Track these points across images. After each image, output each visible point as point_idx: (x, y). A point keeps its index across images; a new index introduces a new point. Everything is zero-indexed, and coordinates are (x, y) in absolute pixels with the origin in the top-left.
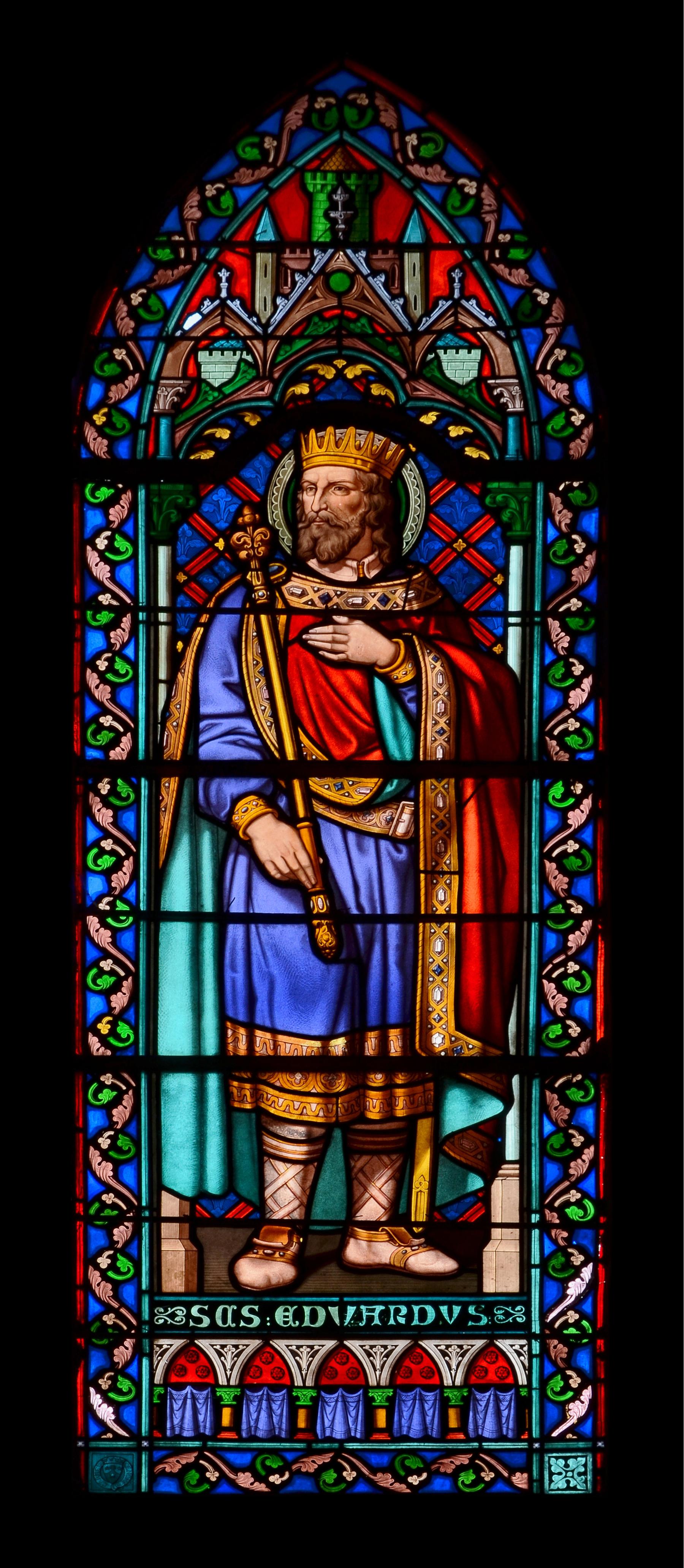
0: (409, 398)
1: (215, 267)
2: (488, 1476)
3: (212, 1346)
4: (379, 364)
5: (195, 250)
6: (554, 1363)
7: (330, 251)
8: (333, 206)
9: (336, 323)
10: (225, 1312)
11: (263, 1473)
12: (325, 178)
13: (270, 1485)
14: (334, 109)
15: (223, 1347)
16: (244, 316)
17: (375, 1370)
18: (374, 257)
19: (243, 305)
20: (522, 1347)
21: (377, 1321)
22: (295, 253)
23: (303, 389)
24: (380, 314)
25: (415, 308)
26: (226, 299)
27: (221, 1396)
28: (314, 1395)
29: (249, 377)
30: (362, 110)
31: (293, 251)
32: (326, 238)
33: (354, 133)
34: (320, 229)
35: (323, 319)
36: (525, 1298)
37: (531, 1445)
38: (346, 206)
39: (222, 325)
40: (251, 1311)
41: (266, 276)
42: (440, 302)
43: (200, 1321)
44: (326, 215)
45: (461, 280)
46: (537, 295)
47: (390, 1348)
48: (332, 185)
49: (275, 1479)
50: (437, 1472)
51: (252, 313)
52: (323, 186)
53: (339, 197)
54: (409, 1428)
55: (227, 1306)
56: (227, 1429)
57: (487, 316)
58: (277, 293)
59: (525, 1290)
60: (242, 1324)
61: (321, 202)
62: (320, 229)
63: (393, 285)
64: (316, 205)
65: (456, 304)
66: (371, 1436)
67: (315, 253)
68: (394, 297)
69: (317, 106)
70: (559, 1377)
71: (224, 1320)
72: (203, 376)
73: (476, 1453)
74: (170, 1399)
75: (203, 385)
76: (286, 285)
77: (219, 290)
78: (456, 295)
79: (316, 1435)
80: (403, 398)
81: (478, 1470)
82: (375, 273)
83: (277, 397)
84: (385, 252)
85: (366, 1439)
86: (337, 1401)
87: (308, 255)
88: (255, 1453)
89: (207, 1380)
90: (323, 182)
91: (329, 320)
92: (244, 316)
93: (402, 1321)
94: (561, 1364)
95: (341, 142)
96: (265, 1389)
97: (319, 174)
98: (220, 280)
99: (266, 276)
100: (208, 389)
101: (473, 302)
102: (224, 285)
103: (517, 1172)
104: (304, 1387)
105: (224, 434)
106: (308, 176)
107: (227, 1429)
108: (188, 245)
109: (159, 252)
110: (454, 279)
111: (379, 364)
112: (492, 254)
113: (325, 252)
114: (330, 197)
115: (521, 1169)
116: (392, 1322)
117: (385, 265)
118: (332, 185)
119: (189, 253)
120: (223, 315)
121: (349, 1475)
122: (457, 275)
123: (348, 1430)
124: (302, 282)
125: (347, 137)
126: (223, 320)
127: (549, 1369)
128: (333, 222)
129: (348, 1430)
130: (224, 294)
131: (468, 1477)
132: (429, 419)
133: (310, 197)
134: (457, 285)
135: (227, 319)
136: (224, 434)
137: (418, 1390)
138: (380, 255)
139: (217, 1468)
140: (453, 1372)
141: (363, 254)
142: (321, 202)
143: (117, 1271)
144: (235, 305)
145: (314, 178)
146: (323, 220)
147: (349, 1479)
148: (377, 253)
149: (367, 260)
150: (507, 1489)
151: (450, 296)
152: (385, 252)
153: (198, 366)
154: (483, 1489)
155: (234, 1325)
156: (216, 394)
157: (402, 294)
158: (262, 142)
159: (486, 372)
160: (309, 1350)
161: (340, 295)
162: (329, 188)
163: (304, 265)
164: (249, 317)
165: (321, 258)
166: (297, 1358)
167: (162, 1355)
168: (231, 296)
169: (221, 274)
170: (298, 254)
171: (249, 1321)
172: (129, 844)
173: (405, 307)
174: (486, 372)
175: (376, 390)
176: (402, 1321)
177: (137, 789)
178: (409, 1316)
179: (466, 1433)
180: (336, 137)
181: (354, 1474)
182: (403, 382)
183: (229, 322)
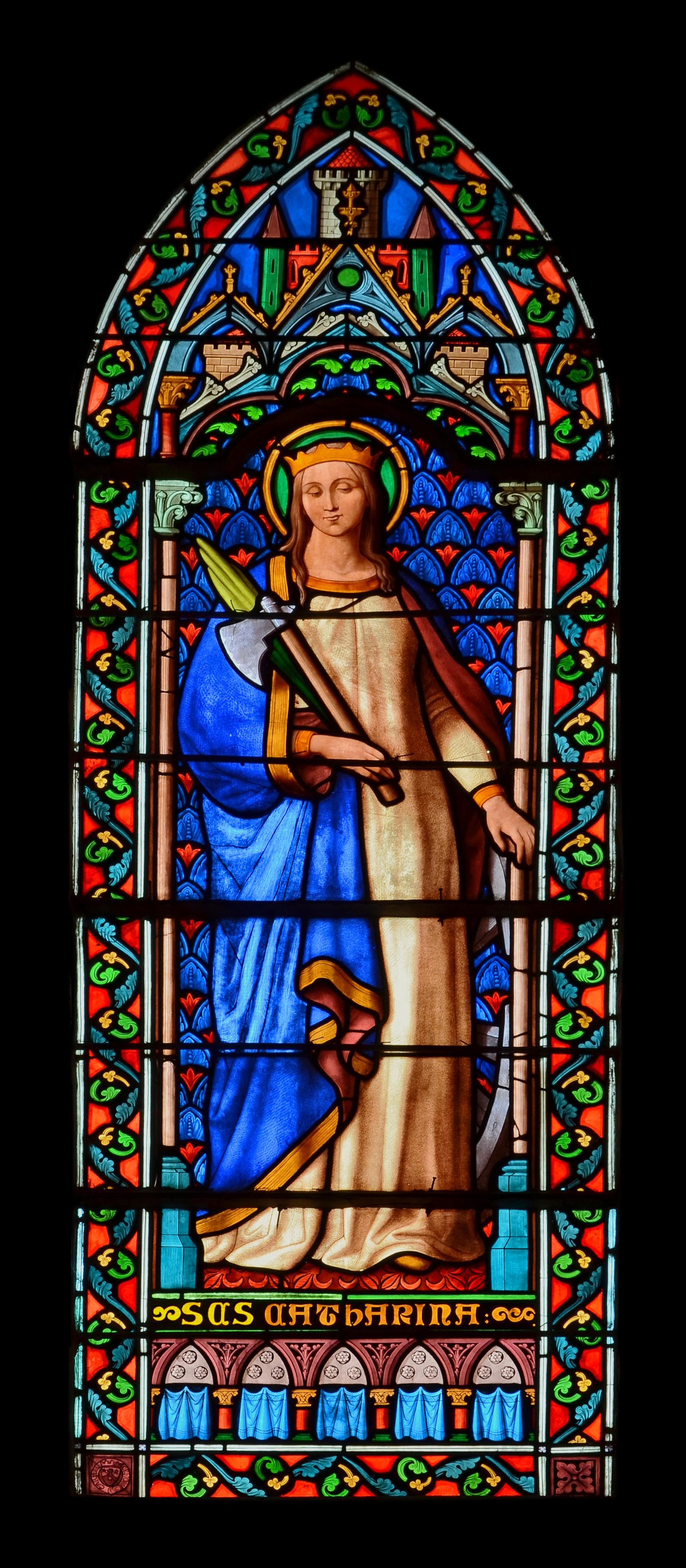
0: (414, 393)
1: (222, 262)
2: (494, 1480)
3: (363, 1344)
4: (387, 360)
5: (197, 247)
6: (562, 1364)
7: (340, 246)
8: (344, 202)
9: (341, 317)
10: (218, 1309)
11: (262, 1477)
12: (334, 176)
13: (270, 1491)
14: (346, 108)
15: (375, 1346)
16: (251, 312)
17: (302, 1370)
18: (382, 252)
19: (250, 302)
20: (529, 1345)
21: (474, 1321)
22: (395, 249)
23: (309, 384)
24: (390, 311)
25: (423, 305)
26: (468, 296)
27: (373, 1398)
28: (314, 1395)
29: (255, 371)
30: (372, 111)
31: (302, 248)
32: (338, 234)
33: (365, 132)
34: (331, 228)
35: (330, 313)
36: (532, 1297)
37: (536, 1449)
38: (357, 202)
39: (228, 320)
40: (245, 1308)
41: (273, 271)
42: (212, 297)
43: (243, 1318)
44: (337, 211)
45: (469, 277)
46: (548, 293)
47: (238, 1347)
48: (342, 184)
49: (275, 1484)
50: (443, 1477)
51: (258, 309)
52: (332, 184)
53: (350, 193)
54: (255, 1430)
55: (220, 1304)
56: (382, 1432)
57: (494, 314)
58: (285, 288)
59: (534, 1288)
60: (235, 1322)
61: (331, 200)
62: (331, 228)
63: (401, 280)
64: (325, 201)
65: (229, 301)
66: (451, 1437)
67: (324, 249)
68: (401, 292)
69: (327, 104)
70: (568, 1377)
71: (274, 1319)
72: (208, 369)
73: (340, 1457)
74: (401, 1401)
75: (208, 379)
76: (293, 280)
77: (225, 285)
78: (465, 292)
79: (473, 1438)
80: (408, 393)
81: (484, 1475)
82: (384, 268)
83: (283, 393)
84: (394, 248)
85: (446, 1442)
86: (494, 1401)
87: (317, 252)
88: (396, 1458)
89: (205, 1381)
90: (366, 180)
91: (335, 314)
92: (251, 312)
93: (407, 1321)
94: (570, 1365)
95: (351, 141)
96: (186, 1389)
97: (328, 172)
98: (226, 276)
99: (273, 271)
100: (212, 382)
101: (244, 299)
102: (230, 282)
103: (525, 1167)
104: (305, 1387)
105: (228, 428)
106: (317, 173)
107: (382, 1432)
108: (191, 242)
109: (164, 249)
110: (463, 275)
111: (387, 360)
112: (503, 252)
113: (334, 248)
114: (339, 194)
115: (529, 1165)
116: (396, 1322)
117: (395, 262)
118: (342, 184)
119: (192, 251)
120: (229, 310)
121: (211, 1481)
122: (466, 272)
123: (505, 1431)
124: (310, 278)
125: (357, 135)
126: (229, 315)
127: (557, 1369)
128: (343, 219)
129: (505, 1431)
130: (465, 292)
131: (474, 1481)
132: (435, 414)
133: (318, 194)
134: (465, 281)
135: (233, 313)
136: (228, 428)
137: (342, 1389)
138: (388, 251)
139: (215, 1473)
140: (305, 1373)
141: (373, 249)
142: (331, 200)
143: (118, 1269)
144: (243, 301)
145: (323, 176)
146: (332, 216)
147: (494, 1484)
148: (385, 248)
149: (376, 255)
150: (231, 1495)
151: (224, 291)
152: (394, 248)
153: (203, 359)
154: (490, 1494)
155: (226, 1323)
156: (220, 388)
157: (410, 290)
158: (272, 139)
159: (494, 369)
160: (461, 1348)
161: (349, 290)
162: (339, 185)
163: (310, 261)
164: (256, 313)
165: (329, 254)
166: (299, 1358)
167: (160, 1354)
168: (473, 292)
169: (227, 271)
170: (308, 252)
171: (243, 1318)
172: (126, 836)
173: (412, 303)
174: (494, 369)
175: (383, 384)
176: (407, 1321)
177: (133, 782)
178: (413, 1317)
179: (393, 1435)
180: (347, 135)
181: (499, 1479)
182: (409, 377)
183: (235, 317)
